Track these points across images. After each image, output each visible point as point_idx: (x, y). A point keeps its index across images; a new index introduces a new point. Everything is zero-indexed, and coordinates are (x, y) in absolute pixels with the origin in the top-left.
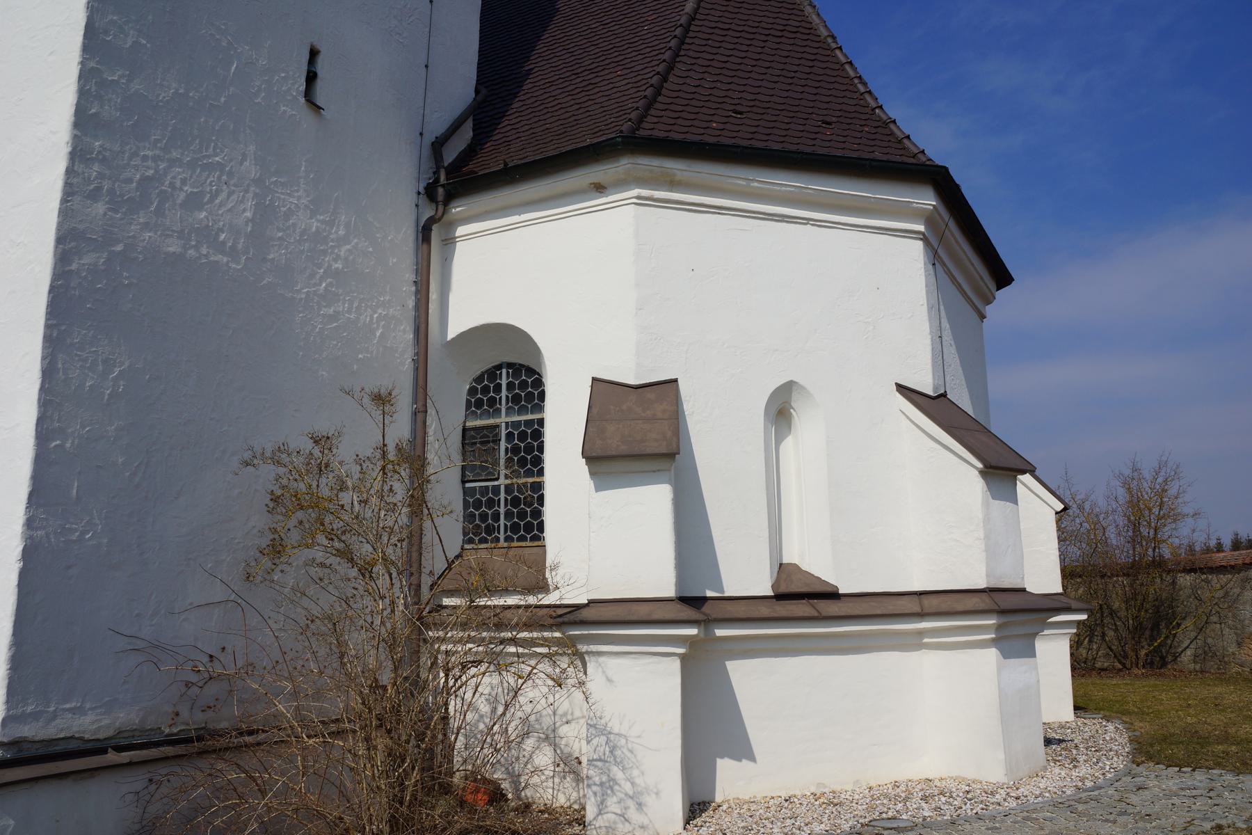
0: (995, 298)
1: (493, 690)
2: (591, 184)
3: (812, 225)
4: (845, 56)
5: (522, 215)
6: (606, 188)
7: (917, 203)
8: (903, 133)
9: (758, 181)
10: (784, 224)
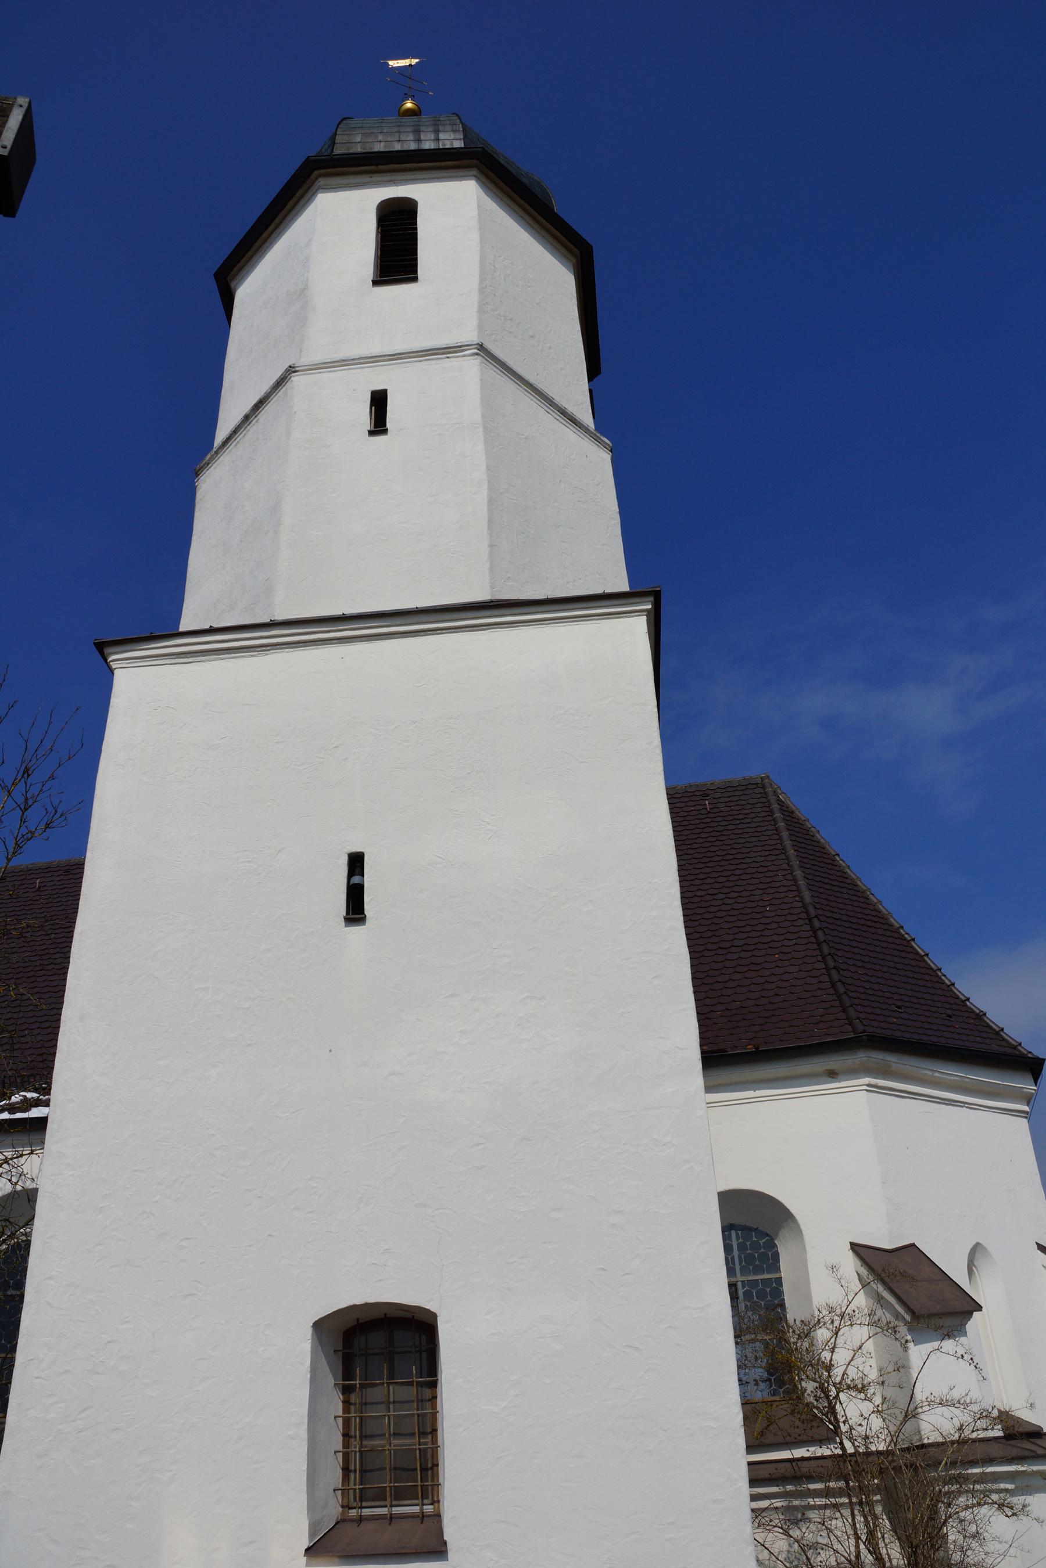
0: (913, 1245)
1: (791, 1547)
2: (826, 1070)
3: (967, 1107)
4: (811, 824)
5: (757, 1091)
6: (837, 1074)
7: (1026, 1088)
8: (950, 981)
9: (939, 1072)
10: (950, 1107)
